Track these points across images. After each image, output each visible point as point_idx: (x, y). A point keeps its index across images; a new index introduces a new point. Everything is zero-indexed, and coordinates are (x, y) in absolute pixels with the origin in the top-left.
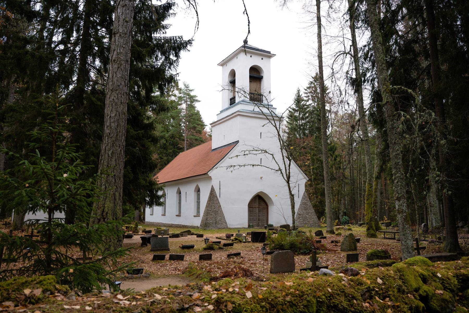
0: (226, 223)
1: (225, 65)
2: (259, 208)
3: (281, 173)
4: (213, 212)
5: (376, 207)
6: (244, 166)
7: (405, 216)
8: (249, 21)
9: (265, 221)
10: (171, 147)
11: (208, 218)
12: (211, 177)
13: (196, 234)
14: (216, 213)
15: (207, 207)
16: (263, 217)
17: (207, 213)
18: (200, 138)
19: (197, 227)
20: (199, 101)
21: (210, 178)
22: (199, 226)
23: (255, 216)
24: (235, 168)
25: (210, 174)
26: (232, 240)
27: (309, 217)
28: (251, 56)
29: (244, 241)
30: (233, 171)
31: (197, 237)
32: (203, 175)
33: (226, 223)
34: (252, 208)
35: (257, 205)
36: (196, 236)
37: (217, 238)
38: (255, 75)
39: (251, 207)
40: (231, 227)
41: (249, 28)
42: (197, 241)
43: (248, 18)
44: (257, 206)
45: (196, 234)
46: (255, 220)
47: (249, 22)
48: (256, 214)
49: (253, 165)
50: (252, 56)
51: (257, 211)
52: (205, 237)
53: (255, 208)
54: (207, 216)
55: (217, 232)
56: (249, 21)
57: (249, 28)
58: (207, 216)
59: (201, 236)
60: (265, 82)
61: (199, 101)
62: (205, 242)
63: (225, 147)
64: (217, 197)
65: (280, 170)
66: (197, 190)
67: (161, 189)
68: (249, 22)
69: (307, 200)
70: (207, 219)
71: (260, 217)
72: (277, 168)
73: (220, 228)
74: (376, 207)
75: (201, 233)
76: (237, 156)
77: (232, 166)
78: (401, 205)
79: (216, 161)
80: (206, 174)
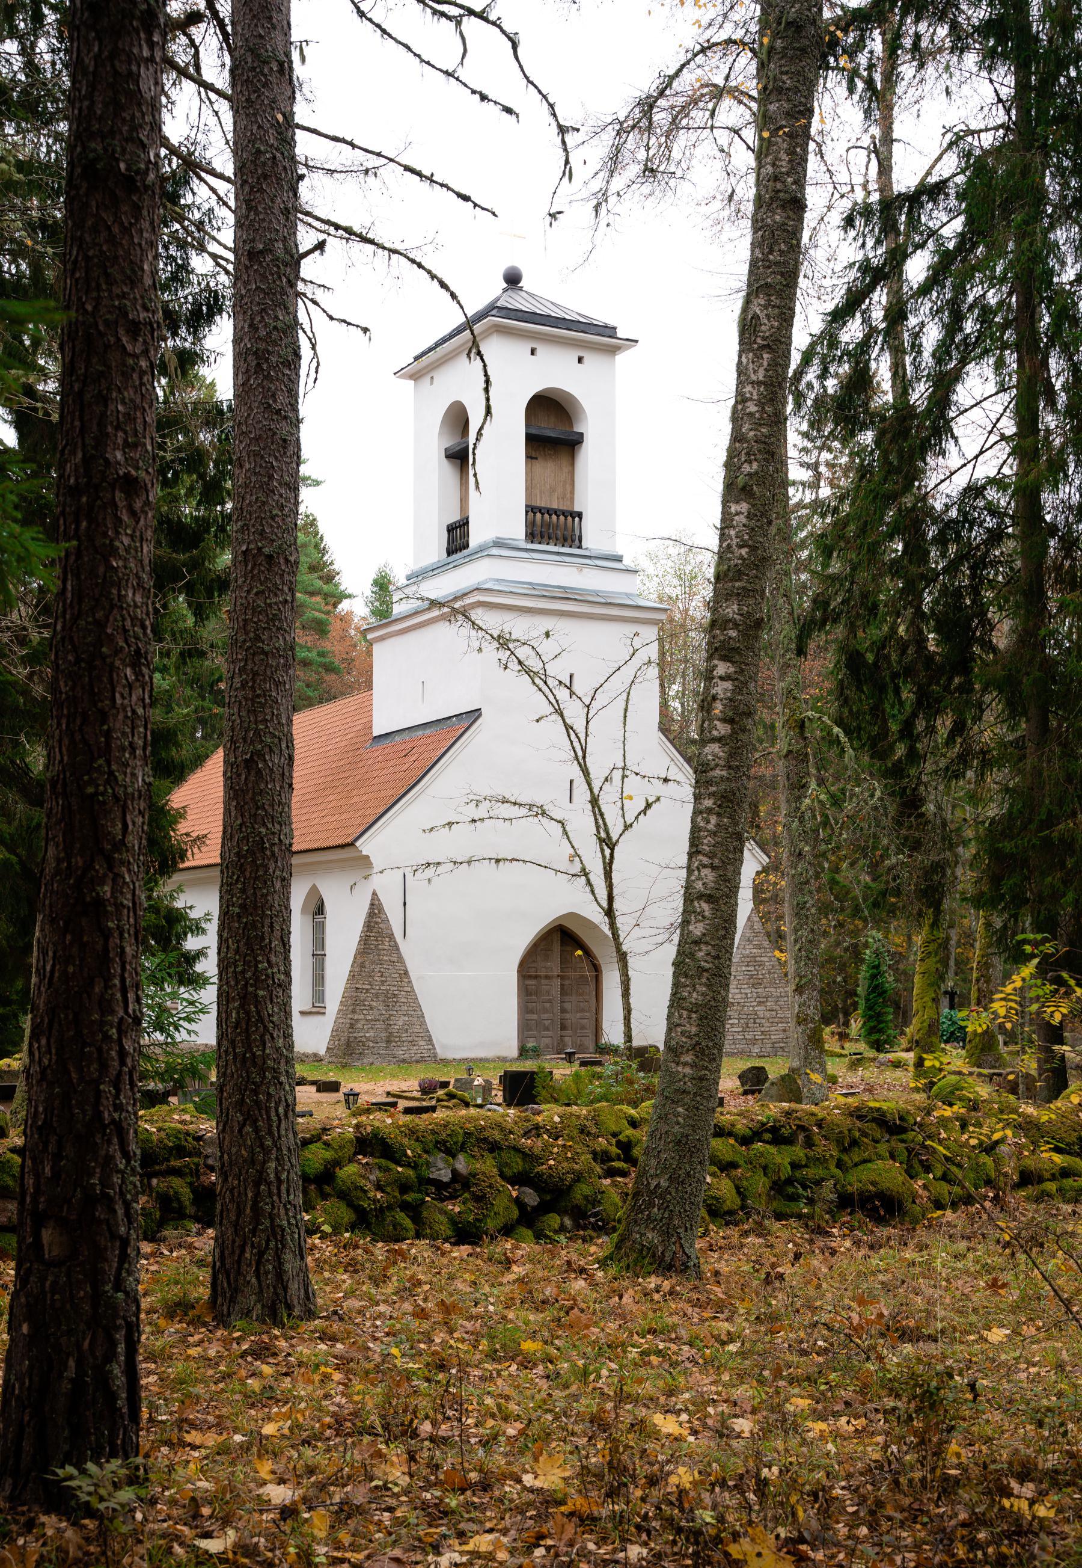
0: (430, 1040)
1: (427, 379)
2: (562, 978)
3: (589, 883)
4: (377, 995)
5: (988, 982)
6: (469, 862)
7: (811, 1029)
8: (486, 375)
9: (590, 1032)
10: (188, 692)
11: (357, 1020)
12: (368, 857)
13: (313, 1083)
14: (390, 999)
15: (352, 976)
16: (579, 1015)
17: (354, 1001)
18: (322, 654)
19: (315, 1055)
20: (317, 483)
21: (365, 862)
22: (322, 1052)
23: (546, 1011)
24: (440, 869)
25: (366, 846)
26: (439, 1100)
27: (768, 1014)
28: (533, 352)
29: (479, 1101)
30: (435, 880)
31: (318, 1091)
32: (339, 851)
33: (430, 1040)
34: (536, 977)
35: (554, 966)
36: (314, 1089)
37: (388, 1094)
38: (549, 428)
39: (530, 977)
40: (450, 1055)
41: (488, 399)
42: (319, 1103)
43: (485, 366)
44: (557, 971)
45: (313, 1083)
46: (547, 1029)
47: (487, 382)
48: (550, 1001)
49: (498, 861)
50: (538, 352)
51: (556, 991)
52: (344, 1089)
53: (547, 977)
54: (354, 1012)
55: (393, 1076)
56: (486, 375)
57: (488, 399)
58: (354, 1012)
59: (334, 1087)
60: (589, 456)
61: (317, 483)
62: (347, 1102)
63: (428, 732)
64: (391, 937)
65: (585, 873)
66: (312, 907)
67: (198, 928)
68: (487, 382)
69: (759, 947)
70: (352, 1026)
71: (568, 1016)
72: (576, 868)
73: (404, 1061)
74: (988, 982)
75: (332, 1077)
76: (450, 824)
77: (429, 864)
78: (804, 1004)
79: (390, 793)
80: (351, 844)
